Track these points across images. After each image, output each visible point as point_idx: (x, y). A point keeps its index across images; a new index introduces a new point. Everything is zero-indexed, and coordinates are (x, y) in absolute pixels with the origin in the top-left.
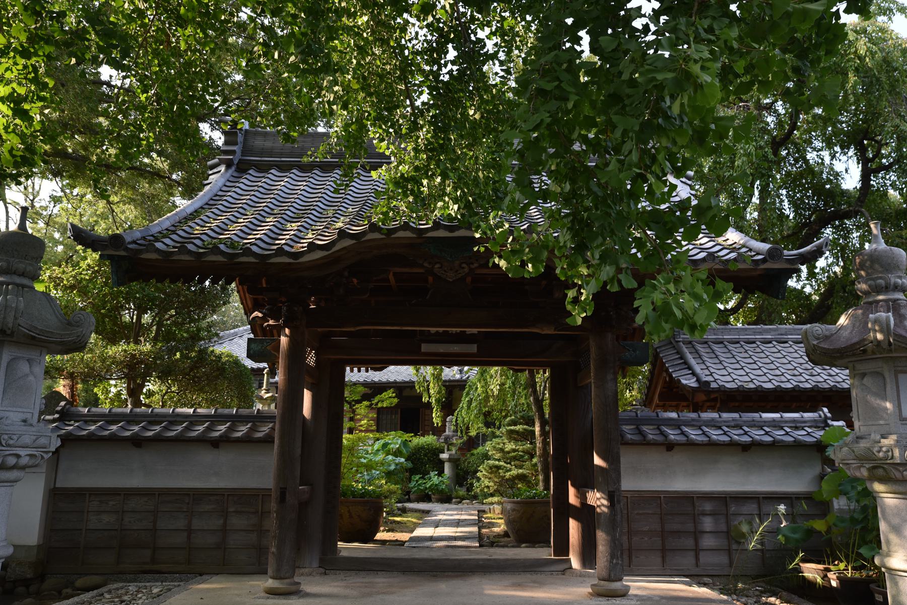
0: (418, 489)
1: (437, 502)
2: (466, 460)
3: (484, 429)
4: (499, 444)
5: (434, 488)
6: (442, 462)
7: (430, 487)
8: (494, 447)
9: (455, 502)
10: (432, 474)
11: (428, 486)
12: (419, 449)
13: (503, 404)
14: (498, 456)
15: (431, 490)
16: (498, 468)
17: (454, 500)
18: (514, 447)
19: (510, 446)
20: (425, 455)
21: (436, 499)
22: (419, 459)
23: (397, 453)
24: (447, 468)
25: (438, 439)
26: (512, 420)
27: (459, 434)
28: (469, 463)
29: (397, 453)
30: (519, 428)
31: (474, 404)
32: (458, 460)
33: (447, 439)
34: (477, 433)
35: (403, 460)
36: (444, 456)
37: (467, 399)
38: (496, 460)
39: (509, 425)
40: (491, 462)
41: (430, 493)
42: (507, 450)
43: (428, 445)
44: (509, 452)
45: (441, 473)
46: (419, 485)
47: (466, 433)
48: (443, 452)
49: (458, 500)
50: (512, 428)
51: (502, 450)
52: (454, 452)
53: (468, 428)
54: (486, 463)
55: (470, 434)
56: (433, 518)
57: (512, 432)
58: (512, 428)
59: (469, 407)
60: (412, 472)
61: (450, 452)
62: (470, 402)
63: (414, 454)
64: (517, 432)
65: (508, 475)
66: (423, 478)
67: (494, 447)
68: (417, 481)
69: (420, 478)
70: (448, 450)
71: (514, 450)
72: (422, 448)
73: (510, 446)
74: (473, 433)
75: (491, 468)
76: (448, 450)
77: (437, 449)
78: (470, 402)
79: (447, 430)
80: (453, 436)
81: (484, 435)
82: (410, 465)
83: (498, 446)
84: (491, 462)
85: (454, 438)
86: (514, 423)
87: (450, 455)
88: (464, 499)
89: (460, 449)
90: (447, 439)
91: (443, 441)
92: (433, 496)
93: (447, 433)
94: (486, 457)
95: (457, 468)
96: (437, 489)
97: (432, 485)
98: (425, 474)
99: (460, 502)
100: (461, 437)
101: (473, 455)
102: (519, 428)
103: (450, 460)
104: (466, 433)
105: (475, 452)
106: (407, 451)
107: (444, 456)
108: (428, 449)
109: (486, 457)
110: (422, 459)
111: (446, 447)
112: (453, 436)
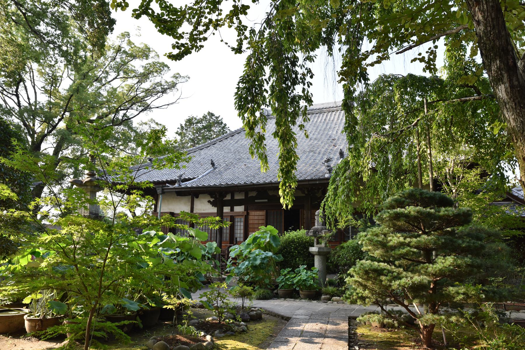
0: (286, 283)
1: (305, 298)
2: (336, 253)
3: (354, 222)
4: (377, 235)
5: (303, 284)
6: (312, 256)
7: (298, 282)
8: (371, 240)
9: (325, 299)
10: (302, 267)
11: (295, 281)
12: (291, 242)
13: (374, 192)
14: (378, 253)
15: (299, 286)
16: (379, 272)
17: (323, 297)
18: (402, 239)
19: (395, 239)
20: (295, 249)
21: (304, 295)
22: (290, 253)
23: (267, 247)
24: (317, 262)
25: (307, 233)
26: (396, 201)
27: (328, 226)
28: (339, 256)
29: (267, 247)
30: (411, 210)
31: (340, 190)
32: (329, 253)
33: (316, 233)
34: (347, 226)
35: (270, 254)
36: (314, 249)
37: (333, 187)
38: (373, 259)
39: (392, 207)
40: (366, 263)
41: (298, 289)
42: (391, 243)
43: (298, 239)
44: (393, 248)
45: (310, 266)
46: (287, 280)
47: (335, 226)
48: (313, 246)
49: (328, 296)
50: (398, 210)
51: (383, 245)
52: (323, 245)
53: (336, 221)
54: (358, 265)
55: (339, 227)
56: (295, 328)
57: (397, 216)
58: (398, 210)
59: (335, 194)
60: (283, 265)
61: (319, 246)
62: (336, 189)
63: (284, 248)
64: (407, 216)
65: (395, 284)
66: (293, 271)
67: (371, 240)
68: (285, 275)
69: (289, 273)
70: (318, 243)
71: (402, 245)
72: (293, 241)
73: (395, 239)
74: (342, 225)
75: (367, 272)
76: (318, 243)
77: (307, 242)
78: (336, 189)
79: (316, 224)
80: (322, 229)
81: (353, 228)
82: (280, 258)
83: (376, 238)
84: (366, 263)
85: (323, 231)
86: (400, 203)
87: (319, 248)
88: (333, 296)
89: (330, 242)
90: (316, 233)
91: (311, 234)
92: (301, 292)
93: (316, 226)
94: (359, 254)
95: (327, 261)
96: (305, 285)
97: (300, 279)
98: (294, 267)
99: (329, 299)
100: (330, 231)
101: (342, 248)
102: (411, 210)
103: (319, 253)
104: (335, 226)
105: (345, 245)
106: (277, 246)
107: (314, 249)
108: (298, 243)
109: (359, 254)
110: (293, 253)
111: (315, 240)
112: (322, 229)
